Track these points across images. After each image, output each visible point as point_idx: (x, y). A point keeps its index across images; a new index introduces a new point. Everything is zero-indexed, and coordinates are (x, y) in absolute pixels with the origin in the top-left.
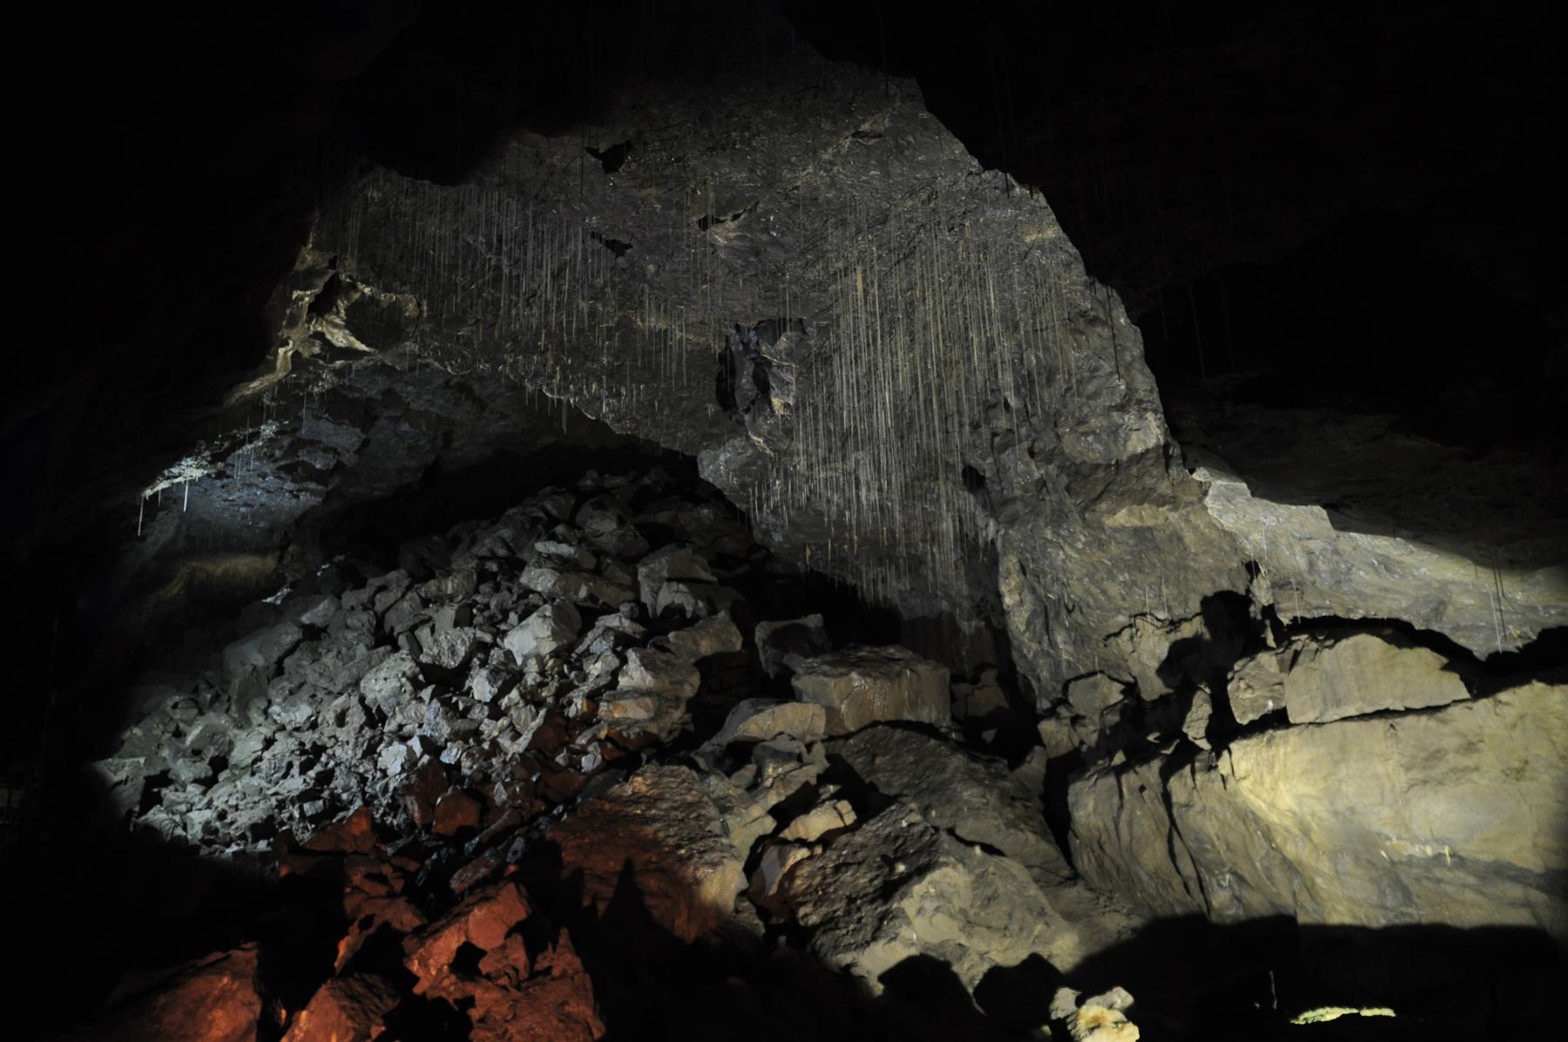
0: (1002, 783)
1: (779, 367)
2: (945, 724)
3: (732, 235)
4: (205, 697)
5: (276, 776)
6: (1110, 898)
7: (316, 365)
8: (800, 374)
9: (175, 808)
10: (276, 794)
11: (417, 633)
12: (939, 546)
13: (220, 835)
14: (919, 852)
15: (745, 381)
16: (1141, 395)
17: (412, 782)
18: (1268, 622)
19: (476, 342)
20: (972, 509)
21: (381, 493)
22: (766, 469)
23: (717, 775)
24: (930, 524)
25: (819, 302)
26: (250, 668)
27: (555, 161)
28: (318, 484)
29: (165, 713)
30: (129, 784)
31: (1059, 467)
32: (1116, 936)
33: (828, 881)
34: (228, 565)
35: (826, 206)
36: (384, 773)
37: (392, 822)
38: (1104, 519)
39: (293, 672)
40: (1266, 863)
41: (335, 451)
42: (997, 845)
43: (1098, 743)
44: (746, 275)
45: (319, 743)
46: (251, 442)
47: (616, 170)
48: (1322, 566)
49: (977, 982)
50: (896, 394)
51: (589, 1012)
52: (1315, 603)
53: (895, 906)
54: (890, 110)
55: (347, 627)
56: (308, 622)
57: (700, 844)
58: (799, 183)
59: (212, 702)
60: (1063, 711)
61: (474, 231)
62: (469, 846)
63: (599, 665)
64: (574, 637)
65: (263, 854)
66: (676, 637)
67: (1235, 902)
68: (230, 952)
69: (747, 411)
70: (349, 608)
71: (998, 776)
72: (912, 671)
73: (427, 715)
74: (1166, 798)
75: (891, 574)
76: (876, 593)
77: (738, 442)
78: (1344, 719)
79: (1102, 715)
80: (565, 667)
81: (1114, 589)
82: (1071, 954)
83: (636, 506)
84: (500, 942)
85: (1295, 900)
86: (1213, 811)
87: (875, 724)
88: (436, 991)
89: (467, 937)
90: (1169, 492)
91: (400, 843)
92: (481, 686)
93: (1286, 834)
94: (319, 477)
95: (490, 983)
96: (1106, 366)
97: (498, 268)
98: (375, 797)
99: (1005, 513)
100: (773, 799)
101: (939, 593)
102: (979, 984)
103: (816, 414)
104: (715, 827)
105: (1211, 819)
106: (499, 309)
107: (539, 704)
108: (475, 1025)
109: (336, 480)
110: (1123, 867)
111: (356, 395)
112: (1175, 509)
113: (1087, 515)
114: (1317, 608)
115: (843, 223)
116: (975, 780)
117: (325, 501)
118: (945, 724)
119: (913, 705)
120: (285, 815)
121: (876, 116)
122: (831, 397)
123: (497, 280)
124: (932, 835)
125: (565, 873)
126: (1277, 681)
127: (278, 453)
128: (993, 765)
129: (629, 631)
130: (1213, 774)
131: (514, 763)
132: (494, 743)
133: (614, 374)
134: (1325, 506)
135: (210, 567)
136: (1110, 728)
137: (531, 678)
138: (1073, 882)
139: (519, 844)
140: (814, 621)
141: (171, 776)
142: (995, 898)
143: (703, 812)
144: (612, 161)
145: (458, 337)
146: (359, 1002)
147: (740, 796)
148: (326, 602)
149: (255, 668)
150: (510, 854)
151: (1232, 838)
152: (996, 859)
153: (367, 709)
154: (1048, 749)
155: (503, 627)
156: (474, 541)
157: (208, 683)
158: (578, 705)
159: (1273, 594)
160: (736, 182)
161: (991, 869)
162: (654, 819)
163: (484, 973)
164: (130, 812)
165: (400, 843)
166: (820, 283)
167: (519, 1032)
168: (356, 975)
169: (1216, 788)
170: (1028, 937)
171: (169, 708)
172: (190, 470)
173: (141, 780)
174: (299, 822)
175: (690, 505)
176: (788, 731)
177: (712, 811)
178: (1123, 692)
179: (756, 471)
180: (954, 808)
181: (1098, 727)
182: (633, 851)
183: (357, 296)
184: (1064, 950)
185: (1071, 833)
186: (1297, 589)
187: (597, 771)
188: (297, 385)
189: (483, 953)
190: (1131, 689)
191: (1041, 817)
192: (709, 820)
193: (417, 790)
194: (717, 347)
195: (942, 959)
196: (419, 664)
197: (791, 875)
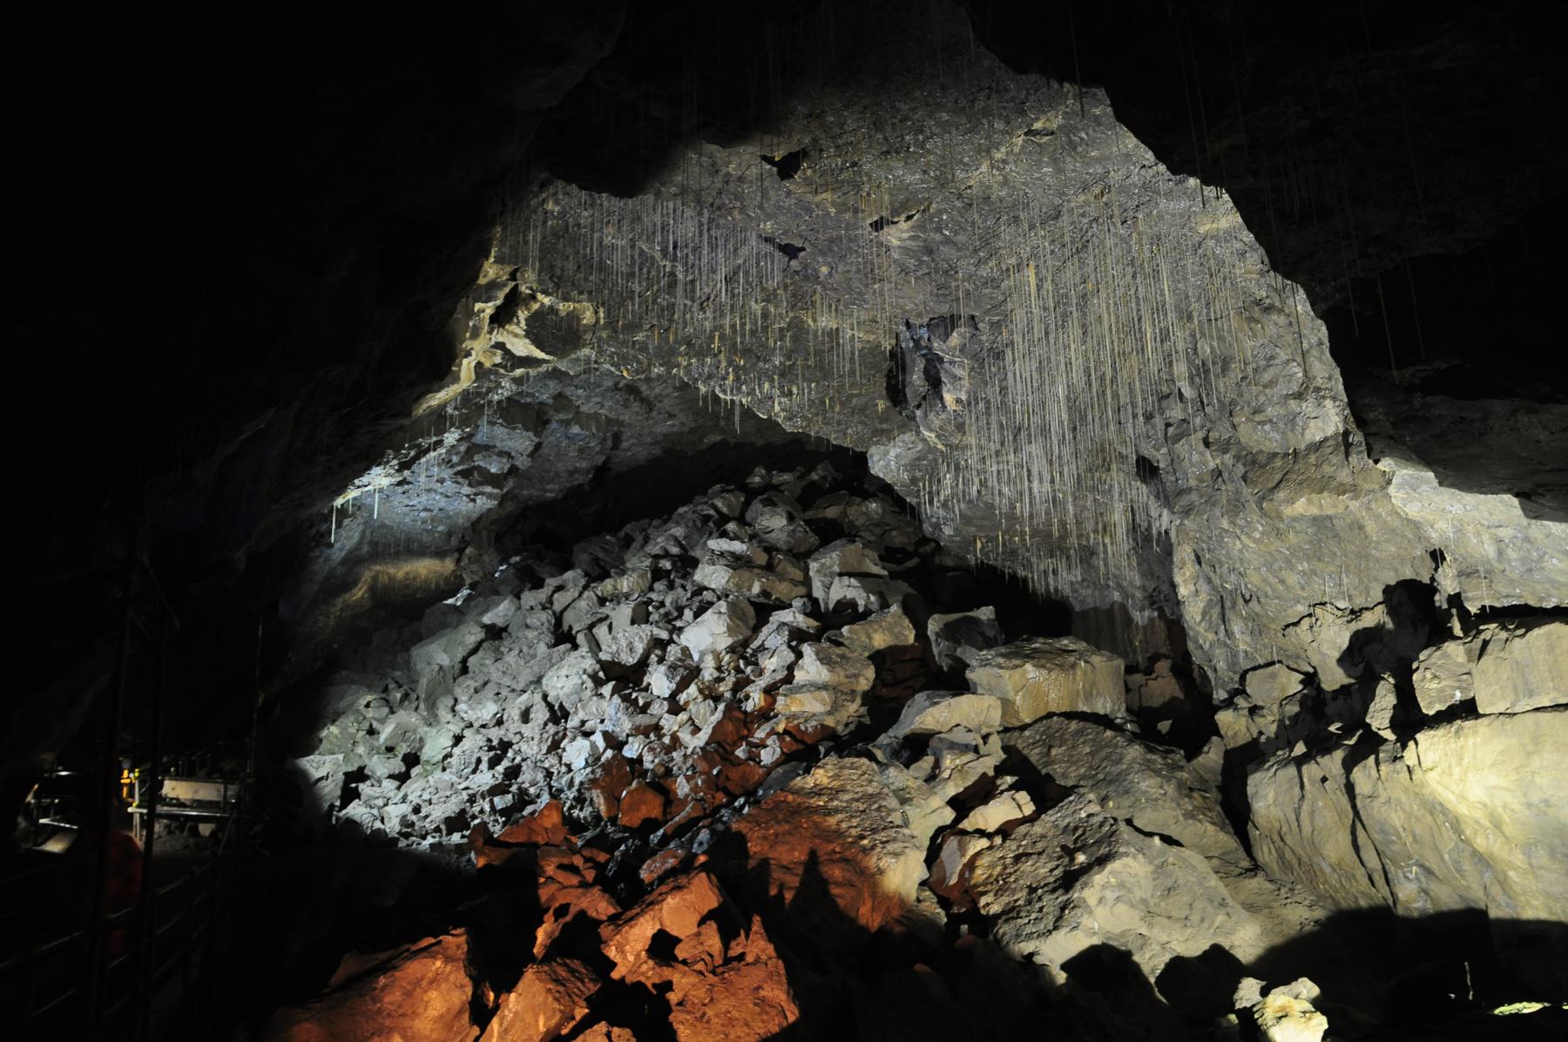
0: (1179, 774)
1: (951, 363)
2: (1120, 715)
3: (905, 235)
4: (395, 696)
5: (466, 771)
6: (1292, 890)
7: (496, 373)
8: (972, 369)
9: (372, 802)
10: (467, 788)
11: (595, 631)
12: (1111, 536)
13: (416, 828)
14: (1098, 842)
15: (916, 379)
16: (1319, 382)
17: (598, 776)
18: (1454, 611)
19: (651, 347)
20: (1145, 499)
21: (553, 495)
22: (937, 464)
23: (896, 767)
24: (1101, 514)
25: (991, 298)
26: (437, 668)
27: (730, 170)
28: (494, 487)
29: (358, 711)
30: (330, 779)
31: (1234, 457)
32: (1299, 928)
33: (1008, 871)
34: (409, 568)
35: (999, 204)
36: (569, 768)
37: (578, 816)
38: (1281, 508)
39: (477, 671)
40: (1455, 856)
41: (509, 455)
42: (1175, 836)
43: (1277, 734)
44: (920, 273)
45: (505, 739)
46: (435, 450)
47: (793, 177)
48: (1512, 554)
49: (1159, 971)
50: (1070, 386)
51: (783, 996)
52: (1504, 591)
53: (1076, 895)
54: (1063, 107)
55: (528, 627)
56: (489, 623)
57: (883, 834)
58: (972, 183)
59: (401, 701)
60: (1239, 700)
61: (650, 239)
62: (654, 838)
63: (774, 659)
64: (750, 633)
65: (458, 846)
66: (850, 631)
67: (1422, 894)
68: (441, 938)
69: (919, 406)
70: (528, 608)
71: (1175, 767)
72: (1086, 662)
73: (608, 711)
74: (1350, 789)
75: (1062, 566)
76: (1047, 584)
77: (908, 437)
78: (1537, 710)
79: (1281, 705)
80: (741, 662)
81: (1292, 579)
82: (1252, 946)
83: (806, 499)
84: (695, 930)
85: (1487, 895)
86: (1399, 802)
87: (1050, 715)
88: (635, 975)
89: (661, 924)
90: (1349, 480)
91: (588, 835)
92: (659, 682)
93: (1476, 827)
94: (494, 481)
95: (687, 968)
96: (1282, 354)
97: (673, 274)
98: (560, 791)
99: (1181, 503)
100: (952, 790)
101: (1111, 584)
102: (1161, 973)
103: (988, 408)
104: (896, 818)
105: (1396, 811)
106: (674, 314)
107: (717, 699)
108: (674, 1008)
109: (510, 483)
110: (1305, 859)
111: (529, 400)
112: (1356, 498)
113: (1264, 505)
114: (1507, 596)
115: (1016, 219)
116: (1152, 770)
117: (501, 504)
118: (1120, 715)
119: (1088, 697)
120: (476, 809)
121: (1049, 114)
122: (1004, 390)
123: (673, 284)
124: (1112, 825)
125: (752, 863)
126: (1465, 671)
127: (455, 459)
128: (1171, 756)
129: (803, 626)
130: (1398, 765)
131: (695, 756)
132: (675, 738)
133: (786, 373)
134: (1517, 495)
135: (392, 570)
136: (1289, 718)
137: (708, 673)
138: (1253, 873)
139: (704, 835)
140: (986, 613)
141: (367, 771)
142: (1175, 889)
143: (884, 804)
144: (787, 168)
145: (634, 342)
146: (564, 985)
147: (919, 788)
148: (506, 602)
149: (441, 667)
150: (695, 845)
151: (1418, 829)
152: (1175, 849)
153: (550, 706)
154: (1226, 740)
155: (678, 624)
156: (646, 540)
157: (396, 682)
158: (755, 699)
159: (1460, 583)
160: (909, 185)
161: (1171, 860)
162: (837, 811)
163: (680, 959)
164: (332, 806)
165: (588, 835)
166: (993, 280)
167: (717, 1015)
168: (558, 960)
169: (1402, 780)
170: (1209, 928)
171: (362, 707)
172: (379, 478)
173: (340, 777)
174: (490, 815)
175: (858, 500)
176: (964, 723)
177: (893, 802)
178: (1302, 682)
179: (926, 466)
180: (1132, 799)
181: (1277, 717)
182: (817, 841)
183: (536, 306)
184: (1247, 942)
185: (1250, 823)
186: (1485, 578)
187: (777, 764)
188: (479, 394)
189: (677, 941)
190: (1310, 679)
191: (1218, 808)
192: (890, 811)
193: (603, 784)
194: (887, 345)
195: (1123, 948)
196: (599, 661)
197: (971, 866)
